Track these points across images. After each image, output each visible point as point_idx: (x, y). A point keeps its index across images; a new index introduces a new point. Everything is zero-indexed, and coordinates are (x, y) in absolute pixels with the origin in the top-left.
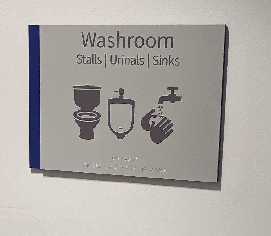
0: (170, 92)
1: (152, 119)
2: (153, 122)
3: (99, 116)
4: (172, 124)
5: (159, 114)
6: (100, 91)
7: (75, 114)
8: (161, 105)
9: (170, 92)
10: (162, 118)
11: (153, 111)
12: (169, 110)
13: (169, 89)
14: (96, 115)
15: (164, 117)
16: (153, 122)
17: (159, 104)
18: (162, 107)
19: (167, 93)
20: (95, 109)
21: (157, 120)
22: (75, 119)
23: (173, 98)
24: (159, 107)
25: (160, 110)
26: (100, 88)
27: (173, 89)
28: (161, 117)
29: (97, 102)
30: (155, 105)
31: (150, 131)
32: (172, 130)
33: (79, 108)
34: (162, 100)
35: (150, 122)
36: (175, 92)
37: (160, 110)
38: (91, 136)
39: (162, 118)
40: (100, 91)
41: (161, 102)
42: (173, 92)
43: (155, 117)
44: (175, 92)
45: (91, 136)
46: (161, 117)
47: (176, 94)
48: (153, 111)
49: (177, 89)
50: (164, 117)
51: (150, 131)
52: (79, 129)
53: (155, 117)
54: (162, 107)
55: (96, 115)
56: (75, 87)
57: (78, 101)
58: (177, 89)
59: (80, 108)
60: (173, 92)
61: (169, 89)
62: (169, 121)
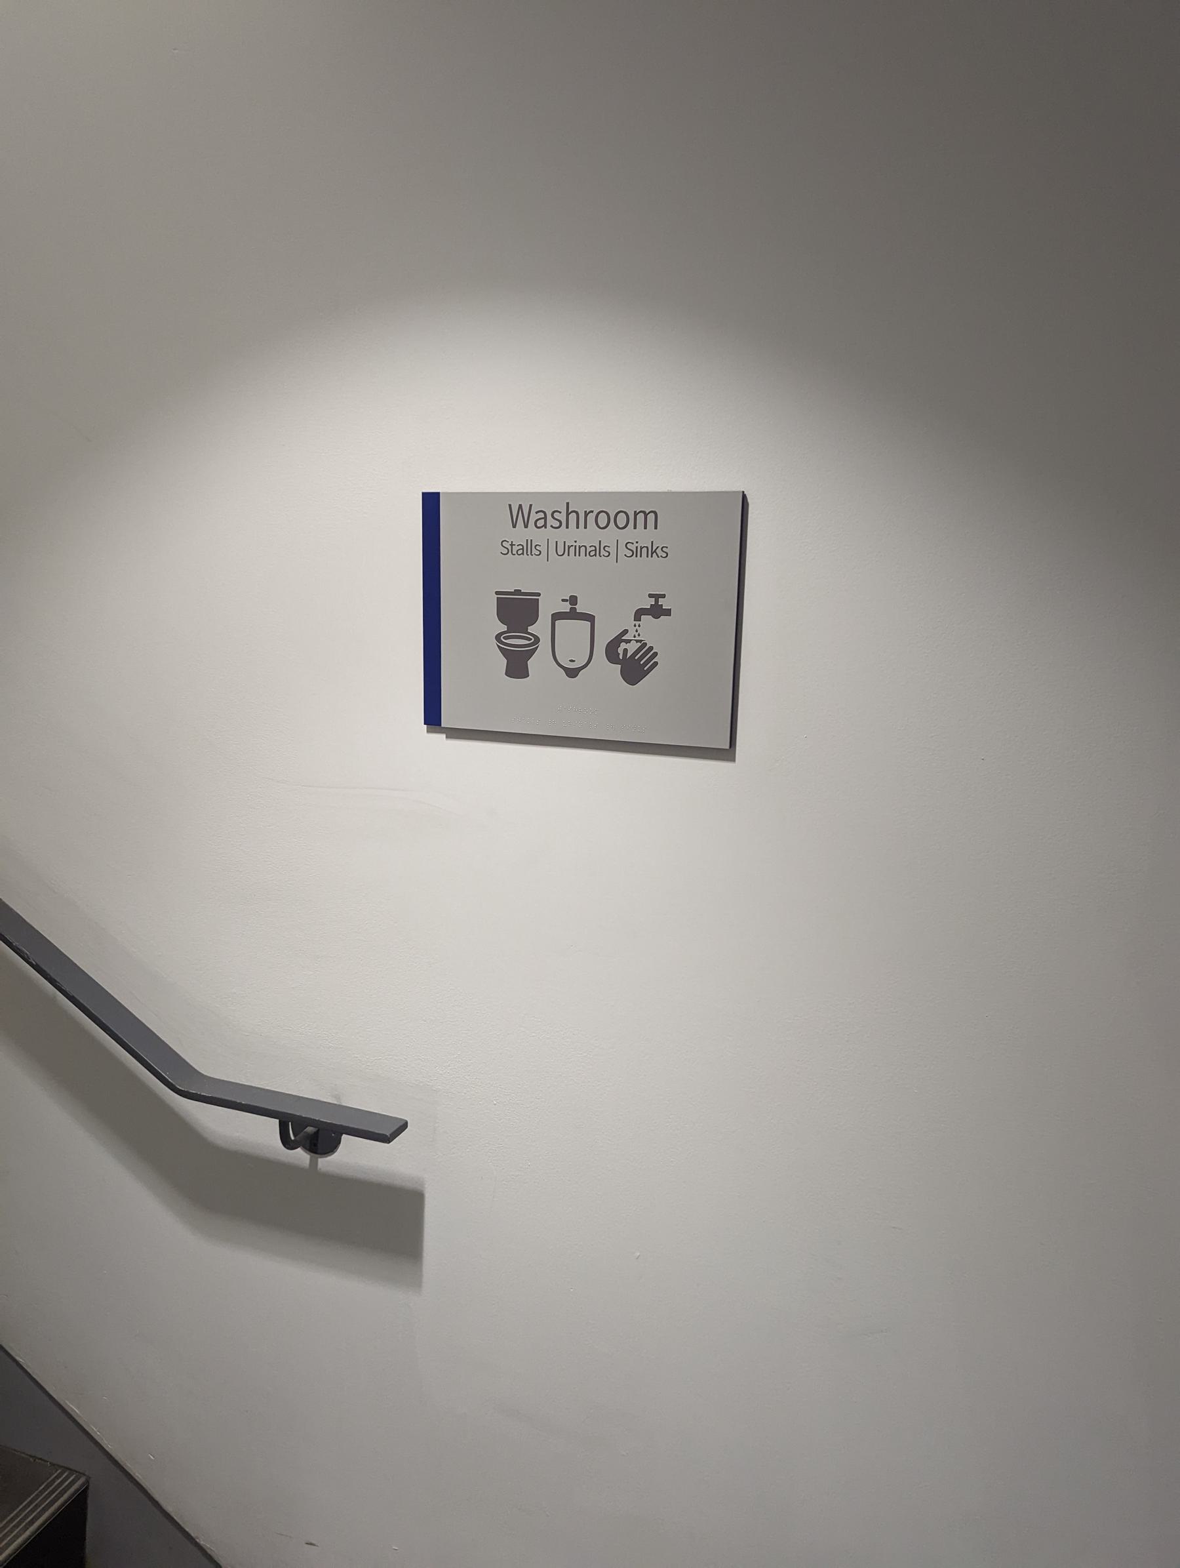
0: (652, 601)
1: (623, 646)
2: (626, 650)
3: (537, 640)
4: (656, 654)
7: (498, 637)
9: (652, 601)
13: (651, 596)
16: (626, 650)
19: (648, 603)
20: (531, 629)
21: (632, 648)
23: (657, 611)
26: (539, 595)
27: (657, 597)
29: (534, 619)
30: (629, 623)
32: (656, 663)
35: (620, 650)
42: (657, 601)
43: (628, 641)
48: (626, 632)
49: (663, 596)
53: (628, 641)
56: (497, 593)
57: (502, 616)
58: (663, 596)
60: (657, 601)
61: (651, 596)
62: (651, 648)
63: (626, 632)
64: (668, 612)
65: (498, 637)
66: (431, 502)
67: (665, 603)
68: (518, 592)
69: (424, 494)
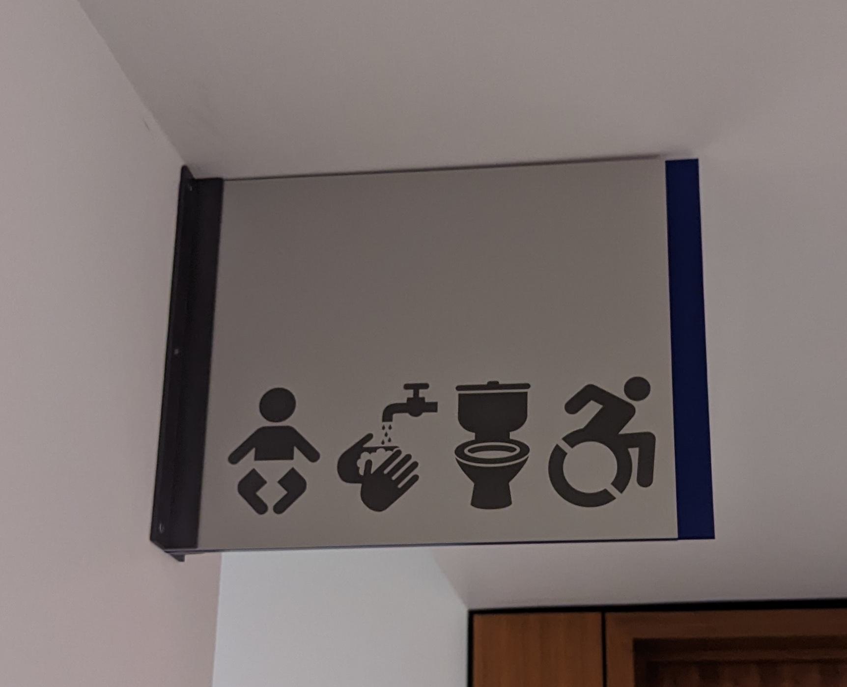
0: (410, 393)
1: (365, 456)
2: (369, 463)
3: (525, 450)
4: (415, 465)
5: (383, 443)
6: (526, 393)
7: (459, 451)
8: (387, 424)
9: (410, 393)
10: (390, 453)
11: (369, 437)
12: (407, 433)
13: (407, 387)
14: (515, 450)
15: (395, 450)
16: (369, 463)
17: (384, 420)
18: (390, 428)
19: (404, 396)
20: (513, 435)
21: (378, 459)
22: (458, 462)
23: (417, 405)
24: (384, 428)
25: (386, 435)
26: (527, 386)
27: (416, 387)
28: (387, 449)
30: (374, 425)
31: (285, 492)
32: (416, 478)
33: (472, 436)
34: (389, 413)
35: (361, 464)
36: (422, 393)
37: (386, 435)
39: (390, 453)
40: (526, 393)
42: (416, 394)
44: (422, 393)
46: (387, 449)
47: (423, 399)
48: (369, 437)
49: (426, 386)
50: (395, 450)
51: (285, 492)
52: (472, 484)
54: (390, 428)
55: (515, 450)
56: (459, 388)
57: (466, 419)
58: (426, 386)
59: (474, 434)
60: (416, 394)
61: (407, 387)
62: (408, 457)
64: (433, 407)
66: (200, 203)
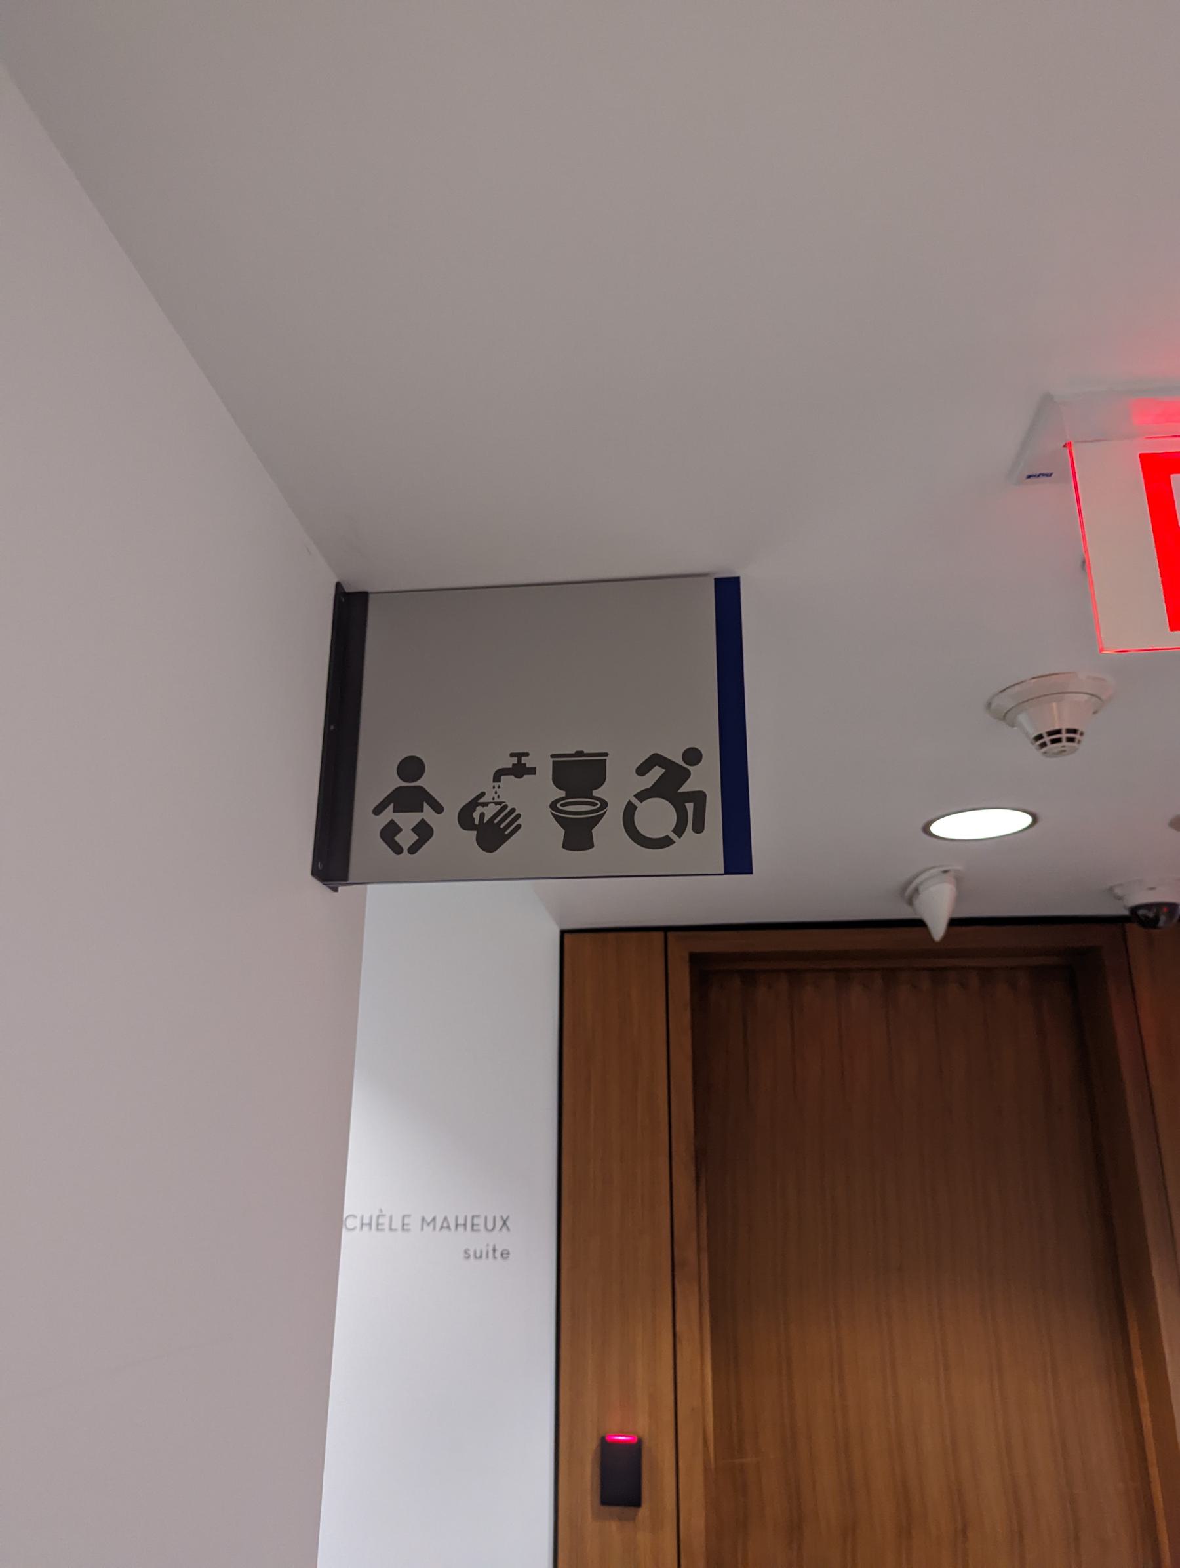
1: (479, 809)
2: (482, 815)
3: (604, 804)
4: (518, 816)
7: (553, 805)
8: (496, 784)
10: (499, 807)
11: (483, 794)
12: (512, 791)
13: (512, 755)
16: (482, 815)
19: (510, 762)
20: (595, 793)
22: (555, 817)
23: (520, 770)
26: (606, 754)
27: (519, 756)
28: (496, 804)
29: (600, 780)
30: (487, 785)
32: (519, 827)
33: (563, 794)
34: (498, 776)
35: (476, 815)
36: (524, 760)
38: (588, 844)
41: (498, 776)
42: (519, 760)
43: (485, 805)
44: (524, 760)
45: (588, 844)
46: (496, 804)
48: (483, 794)
49: (527, 754)
52: (594, 831)
53: (485, 805)
56: (552, 756)
57: (558, 781)
58: (527, 754)
60: (519, 760)
61: (512, 755)
62: (513, 810)
63: (483, 794)
64: (532, 771)
65: (553, 805)
66: (350, 611)
67: (528, 762)
68: (580, 753)
69: (1141, 456)
